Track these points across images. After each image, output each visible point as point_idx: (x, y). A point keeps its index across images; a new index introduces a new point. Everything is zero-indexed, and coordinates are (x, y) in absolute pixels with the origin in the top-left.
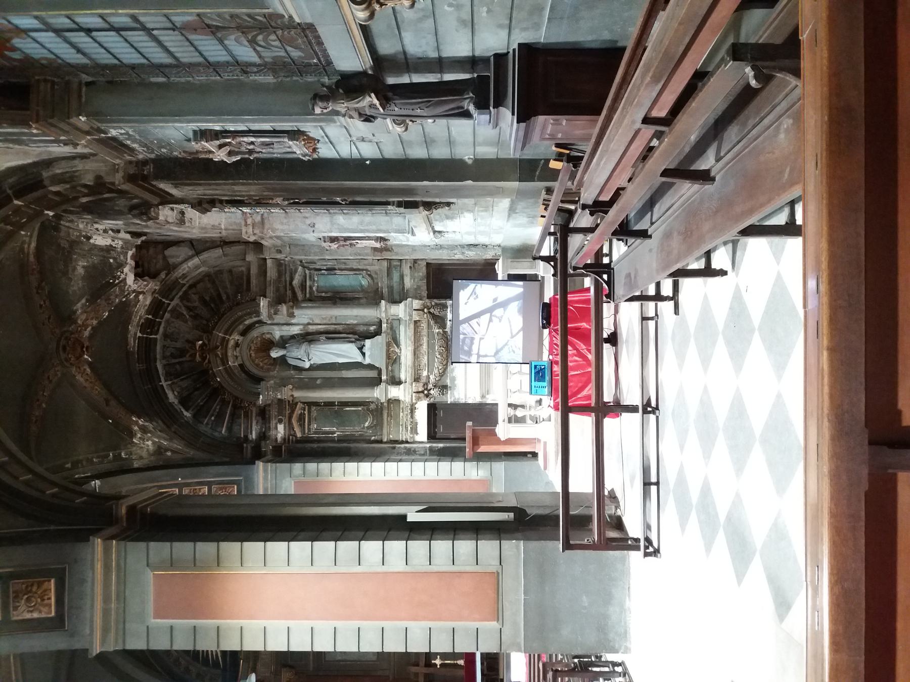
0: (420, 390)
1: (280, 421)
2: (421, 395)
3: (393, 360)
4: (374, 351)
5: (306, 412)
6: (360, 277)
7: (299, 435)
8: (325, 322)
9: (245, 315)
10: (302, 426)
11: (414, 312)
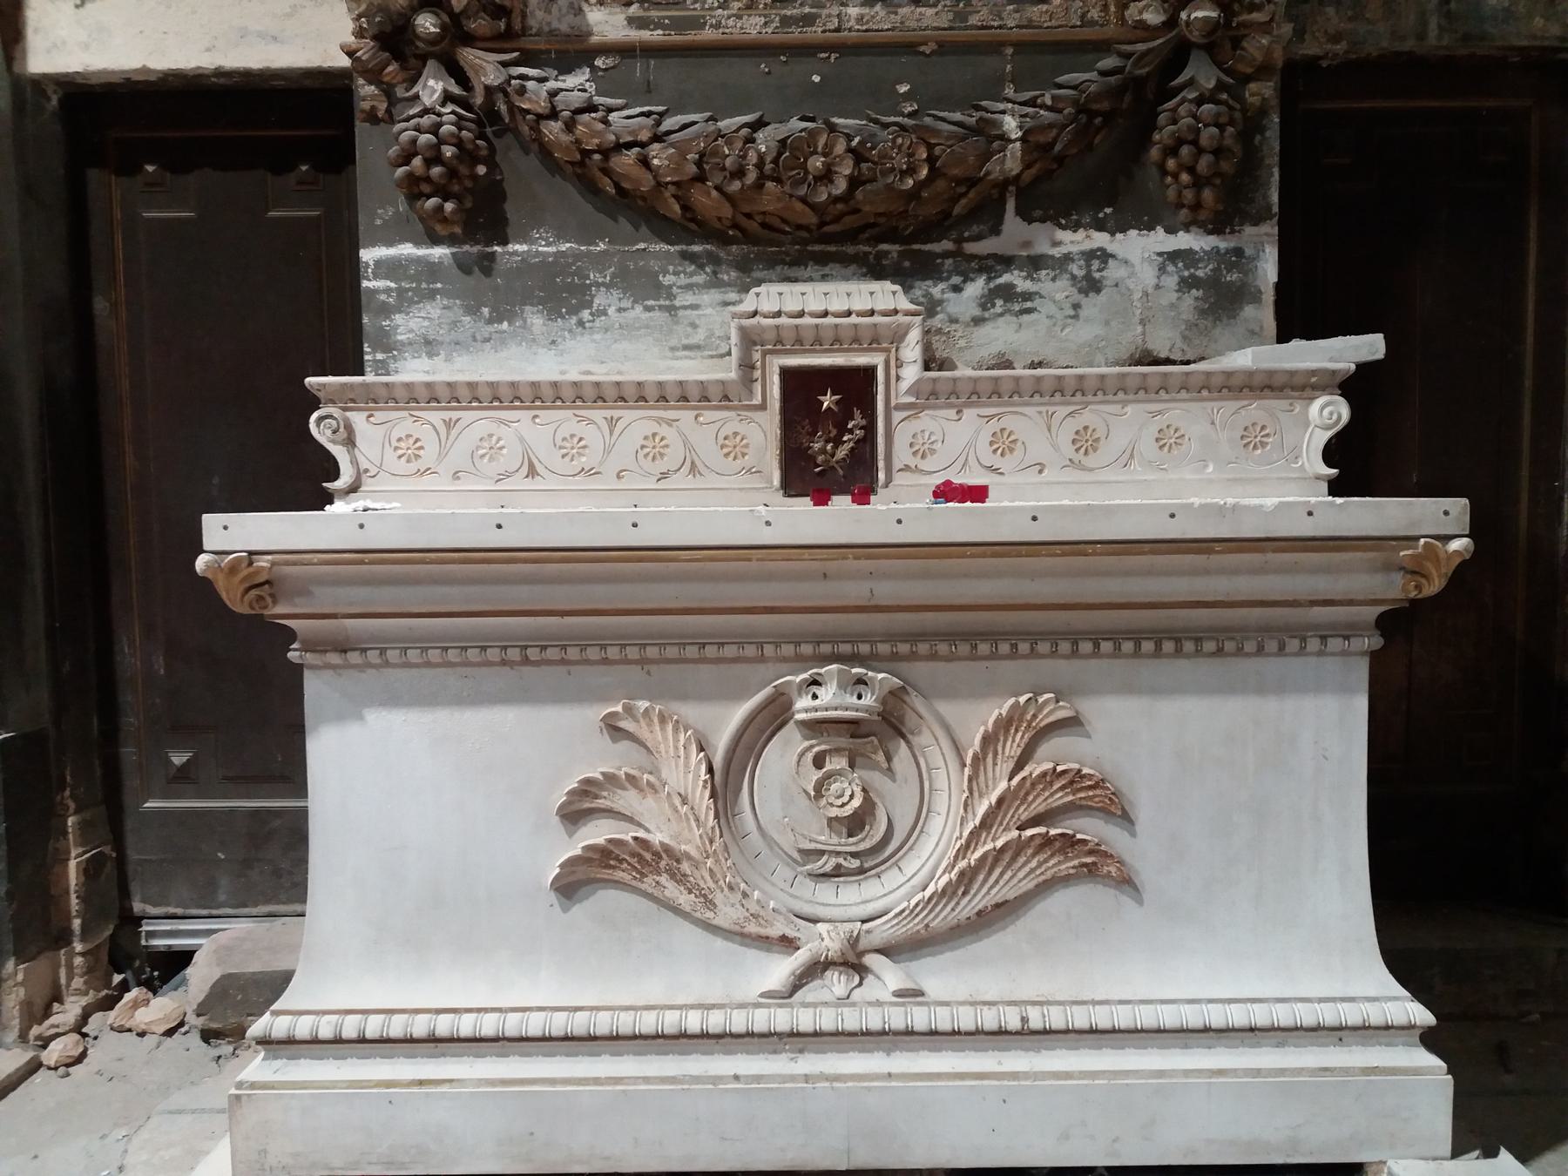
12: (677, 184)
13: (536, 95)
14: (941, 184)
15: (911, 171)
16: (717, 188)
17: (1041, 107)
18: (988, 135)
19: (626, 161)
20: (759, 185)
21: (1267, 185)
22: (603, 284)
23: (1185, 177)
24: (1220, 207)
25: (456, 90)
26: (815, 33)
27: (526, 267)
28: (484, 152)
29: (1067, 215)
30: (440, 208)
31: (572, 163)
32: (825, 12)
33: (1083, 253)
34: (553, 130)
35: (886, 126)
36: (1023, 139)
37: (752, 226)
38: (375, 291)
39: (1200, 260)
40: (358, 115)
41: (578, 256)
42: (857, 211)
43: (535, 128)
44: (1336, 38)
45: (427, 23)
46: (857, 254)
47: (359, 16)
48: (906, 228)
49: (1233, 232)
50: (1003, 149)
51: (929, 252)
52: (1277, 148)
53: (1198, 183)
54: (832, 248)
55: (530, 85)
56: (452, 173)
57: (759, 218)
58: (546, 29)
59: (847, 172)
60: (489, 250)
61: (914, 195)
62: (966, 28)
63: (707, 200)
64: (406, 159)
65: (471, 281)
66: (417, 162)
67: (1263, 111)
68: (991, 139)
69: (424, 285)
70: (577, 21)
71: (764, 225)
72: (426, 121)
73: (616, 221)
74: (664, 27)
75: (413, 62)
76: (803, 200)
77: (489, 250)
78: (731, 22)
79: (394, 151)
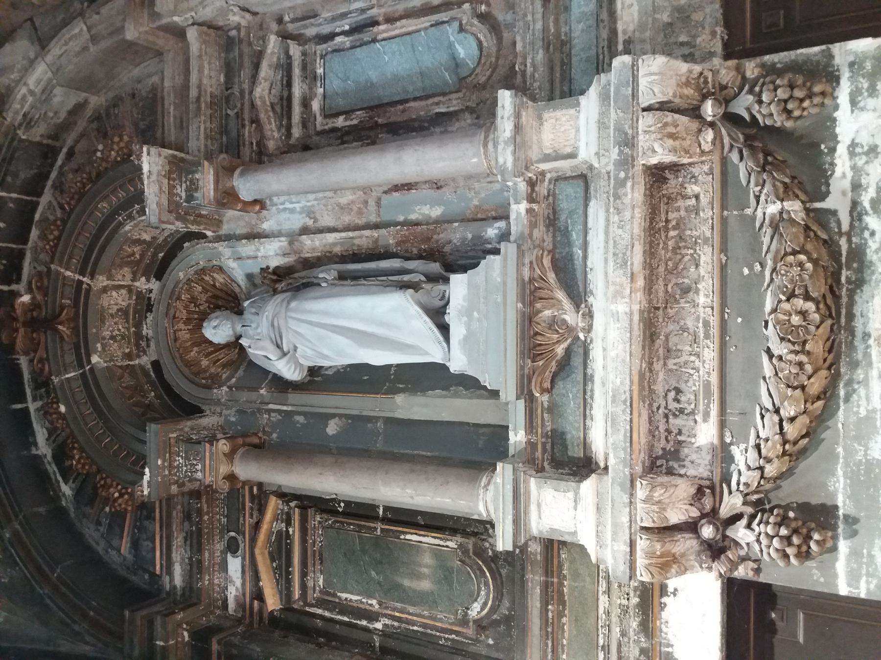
0: (675, 517)
1: (232, 547)
2: (686, 544)
3: (551, 361)
4: (473, 329)
5: (295, 531)
6: (451, 30)
7: (273, 602)
8: (347, 219)
9: (115, 212)
10: (283, 574)
11: (646, 121)
12: (806, 402)
13: (751, 477)
14: (809, 247)
15: (801, 265)
16: (809, 378)
17: (760, 192)
18: (777, 224)
19: (791, 431)
20: (808, 353)
21: (808, 55)
22: (865, 451)
23: (806, 104)
24: (824, 80)
25: (744, 521)
26: (714, 321)
27: (853, 496)
28: (781, 511)
29: (826, 171)
30: (817, 542)
31: (790, 461)
32: (702, 315)
33: (851, 159)
34: (770, 470)
35: (772, 280)
36: (782, 201)
37: (830, 358)
38: (868, 589)
39: (857, 87)
40: (755, 579)
41: (847, 464)
42: (824, 296)
43: (768, 480)
44: (713, 34)
45: (708, 531)
46: (848, 296)
47: (701, 567)
48: (833, 266)
49: (838, 70)
50: (788, 212)
51: (848, 252)
52: (785, 53)
53: (810, 96)
54: (844, 311)
55: (743, 480)
56: (796, 531)
57: (826, 354)
58: (709, 467)
59: (801, 301)
60: (841, 517)
61: (815, 262)
62: (713, 238)
63: (815, 386)
64: (786, 556)
65: (862, 532)
66: (790, 551)
67: (763, 66)
68: (782, 219)
69: (865, 560)
70: (705, 450)
71: (830, 351)
72: (764, 540)
73: (823, 440)
74: (709, 403)
75: (726, 543)
76: (818, 327)
77: (841, 517)
78: (707, 366)
79: (781, 563)
